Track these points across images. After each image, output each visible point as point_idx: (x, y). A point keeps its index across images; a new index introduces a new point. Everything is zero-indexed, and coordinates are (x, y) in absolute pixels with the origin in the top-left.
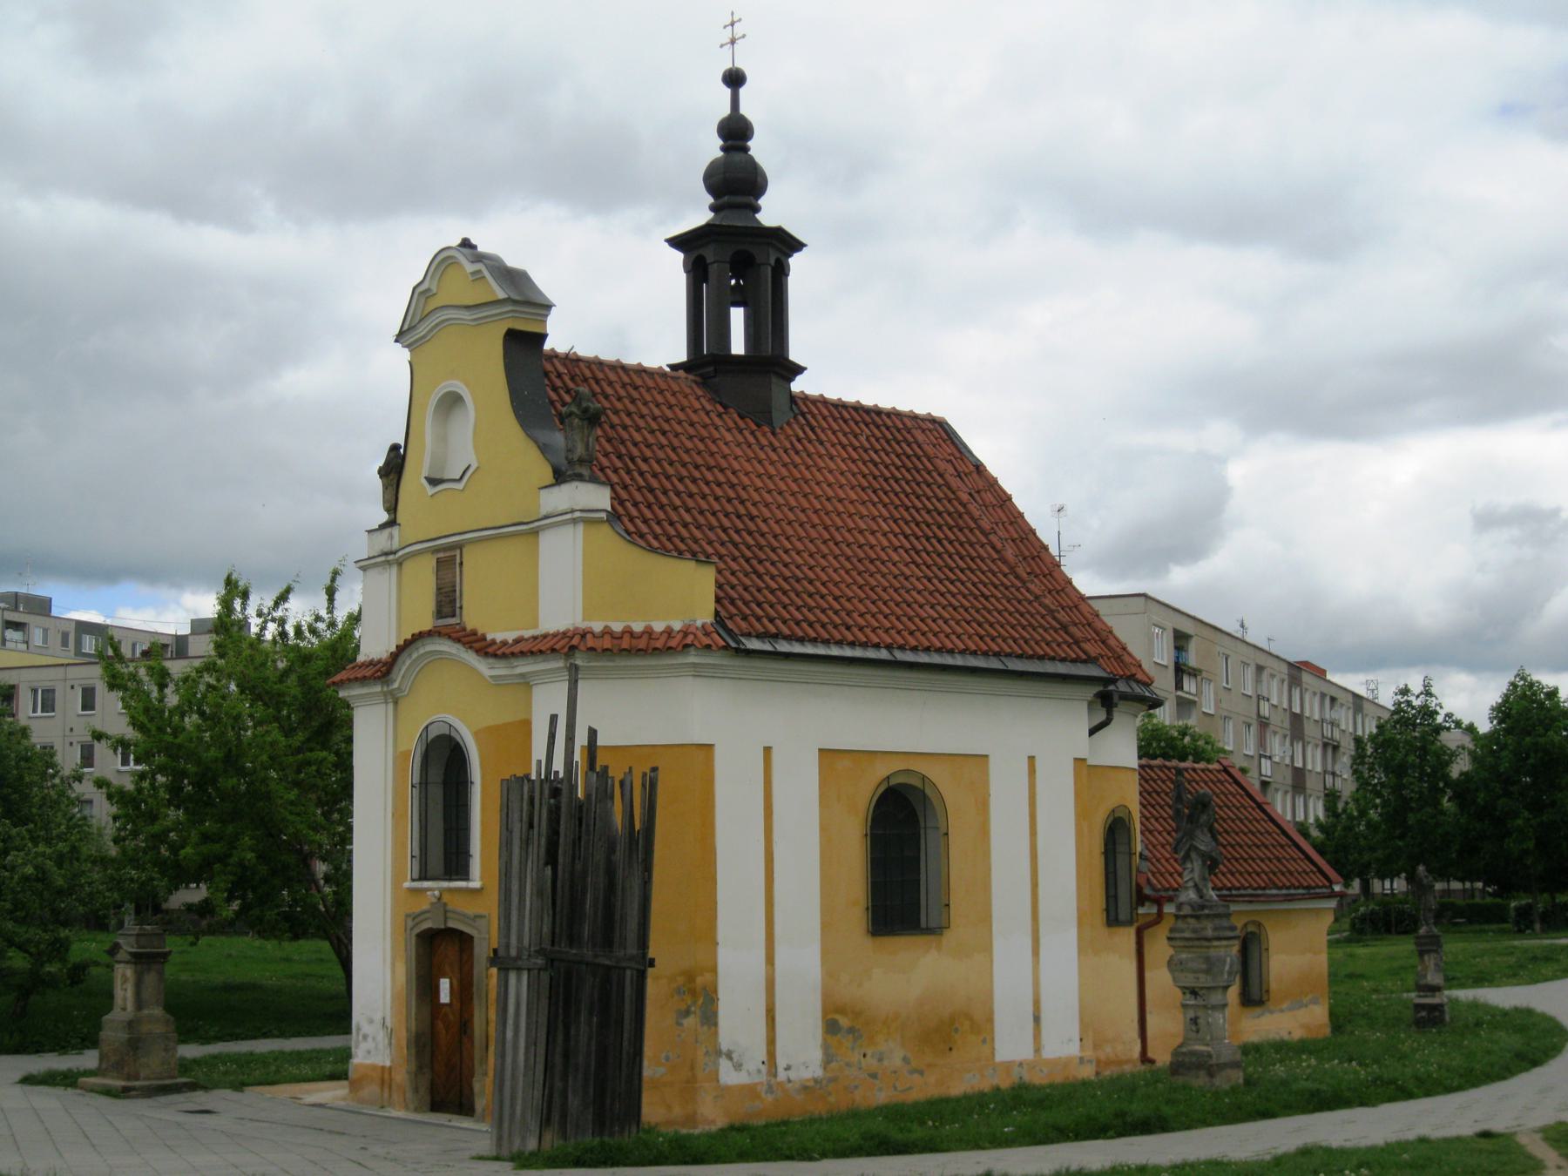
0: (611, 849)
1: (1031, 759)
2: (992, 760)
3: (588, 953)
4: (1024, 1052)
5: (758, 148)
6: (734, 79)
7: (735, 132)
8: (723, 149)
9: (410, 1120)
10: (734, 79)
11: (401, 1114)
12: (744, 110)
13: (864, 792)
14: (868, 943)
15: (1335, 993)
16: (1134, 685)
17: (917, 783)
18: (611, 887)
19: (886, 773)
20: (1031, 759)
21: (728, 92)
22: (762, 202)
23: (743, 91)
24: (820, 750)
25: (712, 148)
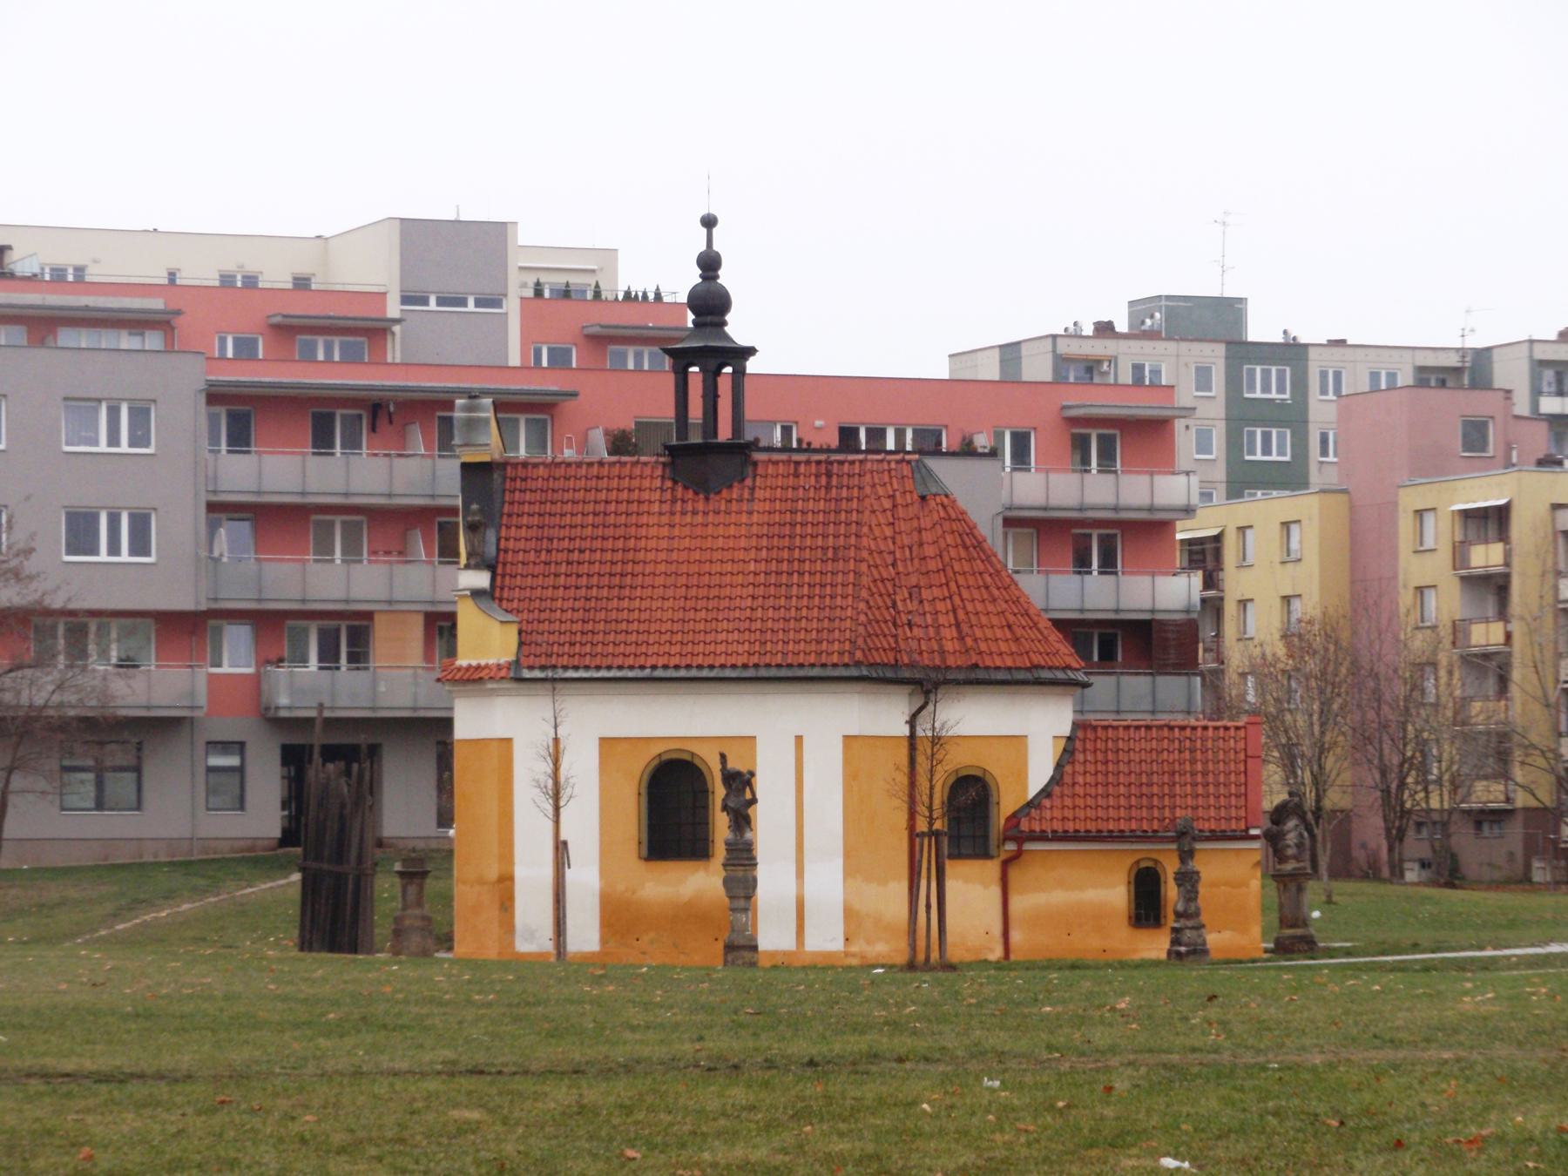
0: (343, 806)
1: (799, 740)
2: (758, 740)
3: (325, 866)
4: (787, 941)
5: (725, 278)
6: (709, 222)
7: (709, 264)
8: (701, 276)
9: (914, 940)
10: (709, 222)
11: (292, 954)
12: (716, 247)
13: (639, 765)
14: (642, 865)
15: (398, 933)
16: (1070, 673)
17: (687, 757)
18: (343, 829)
19: (658, 752)
20: (799, 740)
21: (704, 231)
22: (728, 318)
23: (715, 230)
24: (602, 739)
25: (694, 277)
